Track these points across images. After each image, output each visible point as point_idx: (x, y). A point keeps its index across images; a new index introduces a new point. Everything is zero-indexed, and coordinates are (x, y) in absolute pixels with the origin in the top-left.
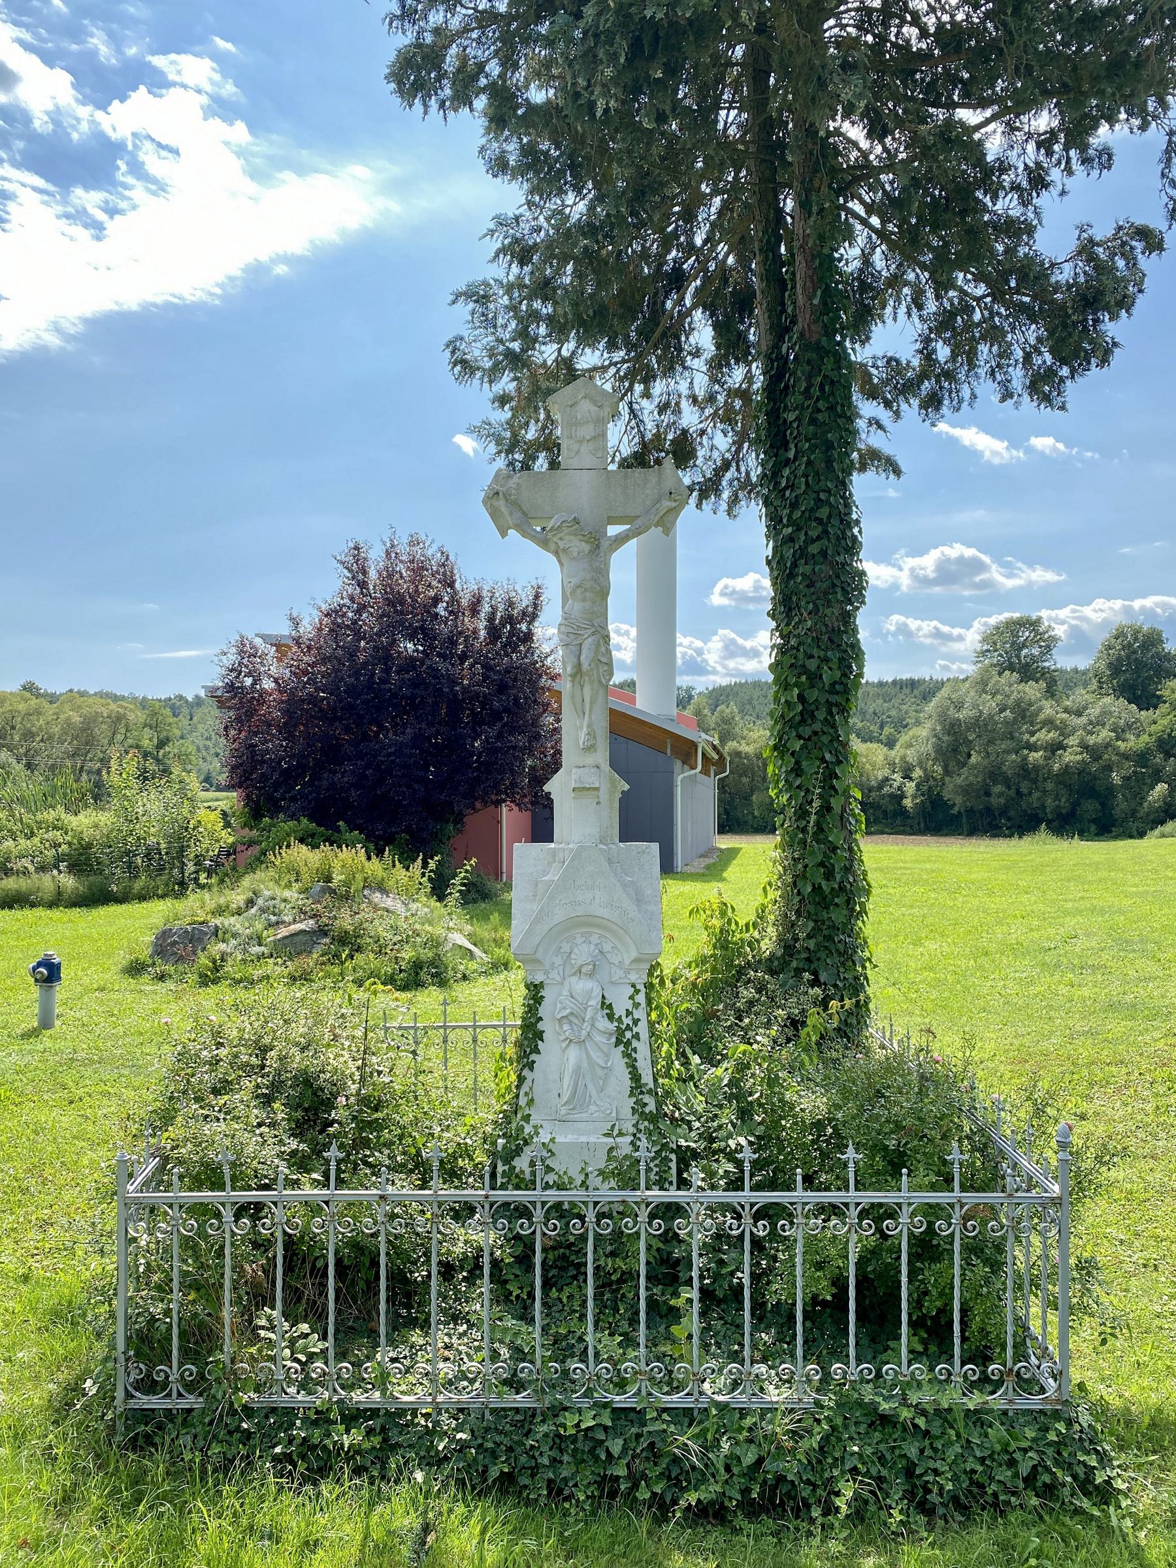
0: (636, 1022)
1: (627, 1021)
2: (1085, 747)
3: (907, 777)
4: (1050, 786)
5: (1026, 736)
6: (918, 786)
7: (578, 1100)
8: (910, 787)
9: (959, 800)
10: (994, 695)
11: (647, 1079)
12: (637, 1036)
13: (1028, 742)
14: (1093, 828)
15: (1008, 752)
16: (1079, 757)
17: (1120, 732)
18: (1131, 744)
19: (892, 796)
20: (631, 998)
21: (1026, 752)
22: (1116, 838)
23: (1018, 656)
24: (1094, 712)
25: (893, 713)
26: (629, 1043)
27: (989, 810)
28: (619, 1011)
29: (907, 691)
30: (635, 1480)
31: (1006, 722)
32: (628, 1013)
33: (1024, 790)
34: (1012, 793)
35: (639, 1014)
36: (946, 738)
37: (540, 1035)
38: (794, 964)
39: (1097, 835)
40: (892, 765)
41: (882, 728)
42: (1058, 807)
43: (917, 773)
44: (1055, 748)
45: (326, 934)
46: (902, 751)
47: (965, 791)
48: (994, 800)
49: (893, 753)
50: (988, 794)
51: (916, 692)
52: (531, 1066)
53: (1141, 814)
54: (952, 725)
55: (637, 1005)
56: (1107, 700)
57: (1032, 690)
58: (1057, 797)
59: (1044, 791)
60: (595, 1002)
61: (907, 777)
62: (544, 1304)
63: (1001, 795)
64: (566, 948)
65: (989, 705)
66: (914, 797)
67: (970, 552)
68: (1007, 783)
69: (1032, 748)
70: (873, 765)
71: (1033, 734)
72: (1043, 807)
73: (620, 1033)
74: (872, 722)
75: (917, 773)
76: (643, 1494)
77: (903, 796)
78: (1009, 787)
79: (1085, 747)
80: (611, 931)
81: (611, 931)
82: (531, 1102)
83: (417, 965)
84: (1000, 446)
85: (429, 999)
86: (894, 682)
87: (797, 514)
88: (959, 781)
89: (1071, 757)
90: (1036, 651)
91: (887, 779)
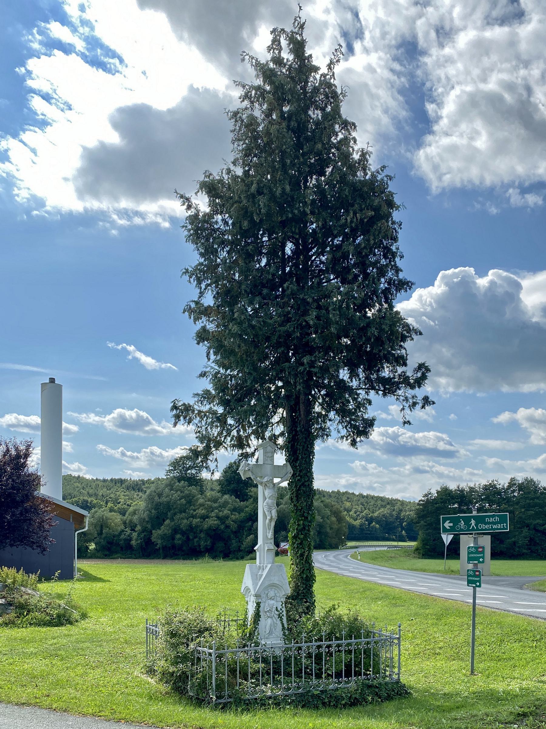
0: (283, 611)
1: (281, 611)
2: (218, 517)
3: (133, 530)
4: (202, 535)
5: (192, 511)
6: (139, 534)
7: (271, 632)
8: (135, 535)
9: (159, 542)
10: (177, 491)
11: (286, 626)
12: (283, 615)
13: (192, 514)
14: (222, 555)
15: (183, 519)
16: (216, 522)
17: (234, 510)
18: (237, 516)
19: (125, 540)
20: (282, 605)
21: (192, 519)
22: (231, 559)
23: (186, 474)
24: (221, 501)
25: (112, 496)
26: (281, 617)
27: (174, 547)
28: (279, 609)
29: (119, 485)
30: (330, 702)
31: (181, 505)
32: (281, 609)
33: (191, 537)
34: (184, 538)
35: (284, 609)
36: (153, 511)
37: (260, 616)
38: (300, 597)
39: (163, 559)
40: (125, 523)
41: (107, 503)
42: (206, 545)
43: (138, 528)
44: (204, 517)
45: (11, 605)
46: (130, 517)
47: (163, 537)
48: (176, 542)
49: (125, 518)
50: (173, 539)
51: (123, 486)
52: (258, 624)
53: (243, 547)
54: (157, 505)
55: (283, 607)
56: (226, 497)
57: (194, 490)
58: (206, 541)
59: (200, 538)
60: (275, 607)
61: (133, 530)
62: (325, 661)
63: (179, 539)
64: (266, 592)
65: (176, 495)
66: (137, 540)
67: (144, 414)
68: (183, 533)
69: (193, 517)
70: (116, 525)
71: (195, 510)
72: (200, 546)
73: (279, 615)
74: (102, 500)
75: (138, 528)
76: (332, 704)
77: (131, 540)
78: (183, 536)
79: (218, 517)
80: (278, 587)
81: (278, 587)
82: (258, 634)
83: (59, 616)
84: (154, 361)
85: (63, 630)
86: (112, 480)
87: (301, 474)
88: (160, 532)
89: (212, 522)
90: (194, 471)
91: (123, 531)
